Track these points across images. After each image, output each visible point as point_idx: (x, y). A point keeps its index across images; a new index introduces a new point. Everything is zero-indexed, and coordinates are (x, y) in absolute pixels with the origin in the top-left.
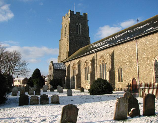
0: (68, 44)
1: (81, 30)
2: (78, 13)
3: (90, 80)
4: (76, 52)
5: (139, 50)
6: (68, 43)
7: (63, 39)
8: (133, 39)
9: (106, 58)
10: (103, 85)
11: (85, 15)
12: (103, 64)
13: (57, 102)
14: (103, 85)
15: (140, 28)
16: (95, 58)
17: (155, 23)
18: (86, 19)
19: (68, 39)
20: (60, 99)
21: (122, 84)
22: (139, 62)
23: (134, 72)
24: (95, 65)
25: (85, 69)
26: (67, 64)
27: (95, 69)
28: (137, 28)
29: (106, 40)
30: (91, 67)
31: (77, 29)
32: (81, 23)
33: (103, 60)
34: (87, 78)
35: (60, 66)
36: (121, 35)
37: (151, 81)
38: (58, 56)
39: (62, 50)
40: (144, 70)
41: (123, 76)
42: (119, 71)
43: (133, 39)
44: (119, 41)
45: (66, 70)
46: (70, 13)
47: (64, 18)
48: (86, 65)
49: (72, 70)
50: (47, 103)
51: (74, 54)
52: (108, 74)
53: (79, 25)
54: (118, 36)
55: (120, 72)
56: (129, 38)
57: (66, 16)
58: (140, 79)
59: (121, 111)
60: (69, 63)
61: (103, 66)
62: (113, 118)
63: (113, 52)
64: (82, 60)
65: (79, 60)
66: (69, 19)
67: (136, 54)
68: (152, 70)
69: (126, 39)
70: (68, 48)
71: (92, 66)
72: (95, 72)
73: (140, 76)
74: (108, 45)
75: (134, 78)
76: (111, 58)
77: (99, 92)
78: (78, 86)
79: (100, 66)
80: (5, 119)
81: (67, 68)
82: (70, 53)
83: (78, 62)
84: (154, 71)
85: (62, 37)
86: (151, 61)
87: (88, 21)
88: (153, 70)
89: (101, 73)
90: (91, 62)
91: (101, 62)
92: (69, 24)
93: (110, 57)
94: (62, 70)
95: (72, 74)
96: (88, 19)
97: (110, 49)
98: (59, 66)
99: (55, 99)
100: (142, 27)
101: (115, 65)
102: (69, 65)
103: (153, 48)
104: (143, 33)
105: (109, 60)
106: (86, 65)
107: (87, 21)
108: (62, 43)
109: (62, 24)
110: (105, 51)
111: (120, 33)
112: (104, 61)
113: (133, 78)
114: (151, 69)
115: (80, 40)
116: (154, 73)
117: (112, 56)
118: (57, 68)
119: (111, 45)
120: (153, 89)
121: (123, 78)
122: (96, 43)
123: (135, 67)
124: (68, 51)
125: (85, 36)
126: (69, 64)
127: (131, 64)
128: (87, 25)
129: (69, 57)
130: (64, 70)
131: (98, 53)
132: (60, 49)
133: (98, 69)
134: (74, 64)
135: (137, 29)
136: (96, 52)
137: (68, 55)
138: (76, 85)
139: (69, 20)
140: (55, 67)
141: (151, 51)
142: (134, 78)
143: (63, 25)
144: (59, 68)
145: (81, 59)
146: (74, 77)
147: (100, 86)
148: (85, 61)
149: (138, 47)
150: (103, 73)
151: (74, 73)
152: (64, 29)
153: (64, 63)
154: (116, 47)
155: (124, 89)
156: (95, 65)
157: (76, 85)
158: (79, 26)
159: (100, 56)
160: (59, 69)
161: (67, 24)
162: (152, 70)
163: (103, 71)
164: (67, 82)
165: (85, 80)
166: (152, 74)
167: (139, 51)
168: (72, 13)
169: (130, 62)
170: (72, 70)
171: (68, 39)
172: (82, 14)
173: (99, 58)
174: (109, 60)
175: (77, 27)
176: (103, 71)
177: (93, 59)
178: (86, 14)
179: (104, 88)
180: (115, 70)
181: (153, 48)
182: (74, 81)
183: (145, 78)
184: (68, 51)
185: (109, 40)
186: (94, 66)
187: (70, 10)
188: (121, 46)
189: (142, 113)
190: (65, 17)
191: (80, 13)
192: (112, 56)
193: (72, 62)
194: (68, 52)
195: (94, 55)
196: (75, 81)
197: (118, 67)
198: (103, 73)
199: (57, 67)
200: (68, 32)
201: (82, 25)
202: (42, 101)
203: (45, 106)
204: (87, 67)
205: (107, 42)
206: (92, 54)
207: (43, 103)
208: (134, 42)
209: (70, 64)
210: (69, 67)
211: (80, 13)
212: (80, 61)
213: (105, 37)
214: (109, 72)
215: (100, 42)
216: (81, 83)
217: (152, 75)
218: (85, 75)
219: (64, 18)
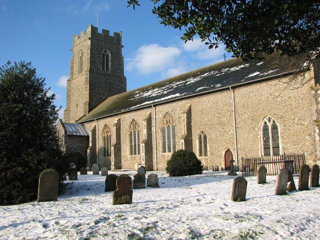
0: (88, 87)
1: (110, 64)
2: (106, 32)
3: (144, 154)
4: (101, 103)
5: (237, 105)
6: (88, 86)
7: (74, 77)
8: (229, 88)
9: (176, 116)
10: (190, 161)
11: (118, 37)
12: (169, 126)
13: (155, 185)
14: (190, 161)
15: (233, 69)
16: (153, 116)
17: (259, 64)
18: (119, 43)
19: (87, 78)
20: (159, 180)
21: (207, 159)
22: (238, 125)
23: (229, 140)
24: (153, 129)
25: (131, 135)
26: (89, 127)
27: (153, 135)
28: (227, 69)
29: (167, 84)
30: (145, 132)
31: (104, 62)
32: (110, 51)
33: (169, 120)
34: (139, 151)
35: (76, 129)
36: (198, 79)
37: (258, 154)
38: (65, 111)
39: (73, 98)
40: (246, 137)
41: (208, 147)
42: (200, 138)
43: (228, 89)
44: (199, 89)
45: (88, 136)
46: (90, 30)
47: (76, 38)
48: (132, 128)
49: (100, 136)
50: (143, 186)
51: (102, 104)
52: (182, 144)
53: (107, 53)
54: (192, 81)
55: (203, 140)
56: (219, 85)
57: (82, 34)
58: (239, 151)
59: (282, 184)
60: (93, 124)
61: (169, 130)
62: (274, 193)
63: (190, 106)
64: (125, 118)
65: (117, 119)
66: (89, 43)
67: (233, 111)
68: (259, 137)
69: (214, 87)
70: (88, 96)
71: (148, 130)
72: (153, 140)
73: (239, 146)
74: (178, 95)
75: (228, 150)
76: (187, 118)
77: (184, 172)
78: (117, 165)
79: (163, 130)
80: (53, 218)
81: (90, 134)
82: (91, 107)
83: (116, 122)
84: (262, 138)
85: (72, 74)
86: (258, 123)
87: (123, 47)
88: (260, 137)
89: (164, 143)
90: (146, 124)
91: (166, 123)
92: (89, 51)
93: (185, 116)
94: (80, 136)
95: (100, 144)
96: (123, 43)
97: (184, 102)
98: (74, 130)
99: (153, 180)
100: (237, 69)
101: (193, 129)
102: (95, 128)
103: (260, 104)
104: (245, 81)
105: (184, 120)
106: (132, 128)
107: (120, 46)
108: (72, 86)
109: (73, 49)
110: (174, 104)
111: (194, 75)
112: (171, 122)
113: (226, 150)
114: (258, 135)
115: (108, 82)
116: (262, 142)
117: (189, 113)
118: (72, 132)
119: (185, 95)
120: (278, 164)
121: (208, 149)
122: (146, 89)
123: (229, 133)
124: (88, 101)
125: (118, 74)
126: (94, 126)
127: (223, 128)
128: (121, 54)
129: (90, 111)
130: (84, 136)
131: (158, 108)
132: (67, 96)
133: (160, 135)
134: (106, 125)
135: (228, 70)
136: (155, 106)
137: (88, 108)
138: (113, 164)
139: (90, 43)
140: (68, 130)
141: (258, 109)
142: (228, 150)
143: (75, 51)
144: (76, 132)
145: (122, 117)
146: (105, 148)
147: (185, 163)
148: (131, 120)
149: (237, 100)
150: (169, 142)
151: (105, 141)
152: (77, 60)
153: (82, 123)
154: (196, 100)
155: (212, 168)
156: (153, 129)
157: (113, 164)
158: (107, 55)
159: (164, 113)
160: (75, 134)
161: (84, 51)
162: (259, 137)
163: (169, 138)
164: (91, 159)
165: (132, 154)
166: (260, 143)
167: (237, 108)
168: (94, 30)
169: (220, 123)
170: (100, 136)
171: (87, 78)
172: (111, 34)
173: (161, 116)
174: (184, 120)
175: (103, 57)
176: (169, 138)
177: (148, 118)
178: (120, 35)
179: (193, 166)
180: (193, 136)
181: (260, 104)
182: (108, 156)
183: (247, 150)
184: (87, 101)
185: (174, 85)
186: (151, 130)
187: (92, 26)
188: (205, 98)
189: (297, 188)
190: (79, 38)
191: (109, 31)
192: (189, 113)
193: (102, 123)
194: (88, 103)
195: (152, 110)
196: (111, 156)
197: (199, 132)
198: (169, 142)
199: (71, 130)
200: (86, 66)
201: (112, 54)
202: (138, 184)
203: (141, 190)
204: (135, 132)
205: (171, 89)
206: (146, 110)
207: (137, 186)
208: (230, 94)
209: (95, 126)
210: (94, 131)
211: (109, 31)
212: (119, 120)
213: (165, 79)
214: (183, 140)
215: (159, 85)
216: (123, 161)
217: (259, 145)
218: (131, 146)
219: (76, 38)
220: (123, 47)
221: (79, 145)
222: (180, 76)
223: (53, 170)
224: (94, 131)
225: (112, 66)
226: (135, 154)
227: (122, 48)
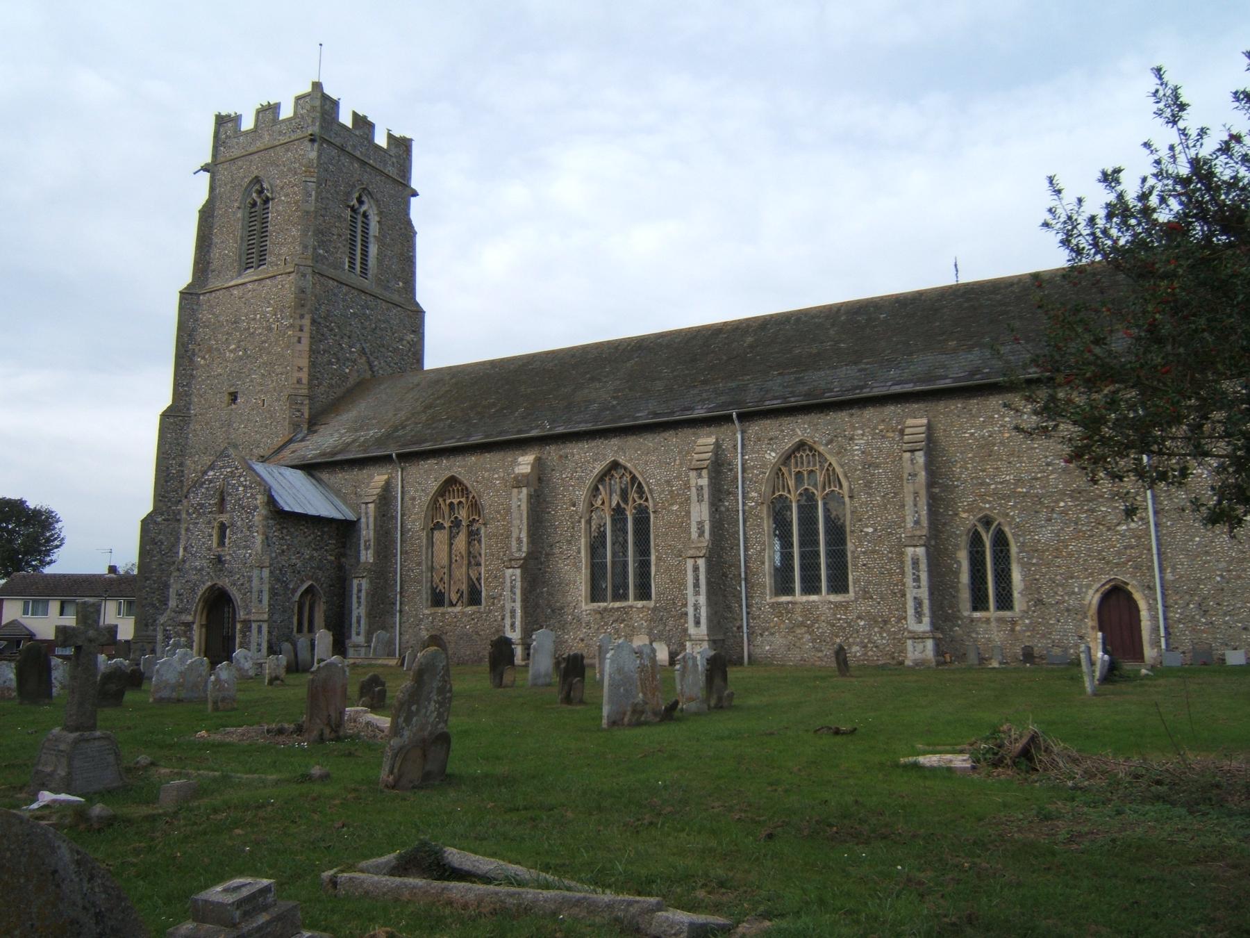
1: (373, 250)
2: (363, 123)
3: (702, 599)
11: (402, 146)
23: (1119, 553)
87: (415, 194)
131: (755, 428)
158: (365, 215)
201: (380, 213)
220: (415, 194)
221: (312, 557)
222: (689, 328)
223: (436, 648)
224: (385, 498)
225: (380, 261)
226: (620, 595)
227: (413, 200)
